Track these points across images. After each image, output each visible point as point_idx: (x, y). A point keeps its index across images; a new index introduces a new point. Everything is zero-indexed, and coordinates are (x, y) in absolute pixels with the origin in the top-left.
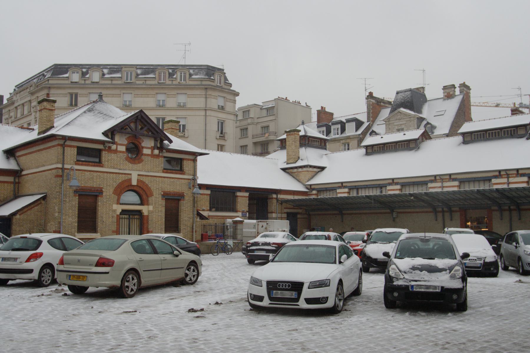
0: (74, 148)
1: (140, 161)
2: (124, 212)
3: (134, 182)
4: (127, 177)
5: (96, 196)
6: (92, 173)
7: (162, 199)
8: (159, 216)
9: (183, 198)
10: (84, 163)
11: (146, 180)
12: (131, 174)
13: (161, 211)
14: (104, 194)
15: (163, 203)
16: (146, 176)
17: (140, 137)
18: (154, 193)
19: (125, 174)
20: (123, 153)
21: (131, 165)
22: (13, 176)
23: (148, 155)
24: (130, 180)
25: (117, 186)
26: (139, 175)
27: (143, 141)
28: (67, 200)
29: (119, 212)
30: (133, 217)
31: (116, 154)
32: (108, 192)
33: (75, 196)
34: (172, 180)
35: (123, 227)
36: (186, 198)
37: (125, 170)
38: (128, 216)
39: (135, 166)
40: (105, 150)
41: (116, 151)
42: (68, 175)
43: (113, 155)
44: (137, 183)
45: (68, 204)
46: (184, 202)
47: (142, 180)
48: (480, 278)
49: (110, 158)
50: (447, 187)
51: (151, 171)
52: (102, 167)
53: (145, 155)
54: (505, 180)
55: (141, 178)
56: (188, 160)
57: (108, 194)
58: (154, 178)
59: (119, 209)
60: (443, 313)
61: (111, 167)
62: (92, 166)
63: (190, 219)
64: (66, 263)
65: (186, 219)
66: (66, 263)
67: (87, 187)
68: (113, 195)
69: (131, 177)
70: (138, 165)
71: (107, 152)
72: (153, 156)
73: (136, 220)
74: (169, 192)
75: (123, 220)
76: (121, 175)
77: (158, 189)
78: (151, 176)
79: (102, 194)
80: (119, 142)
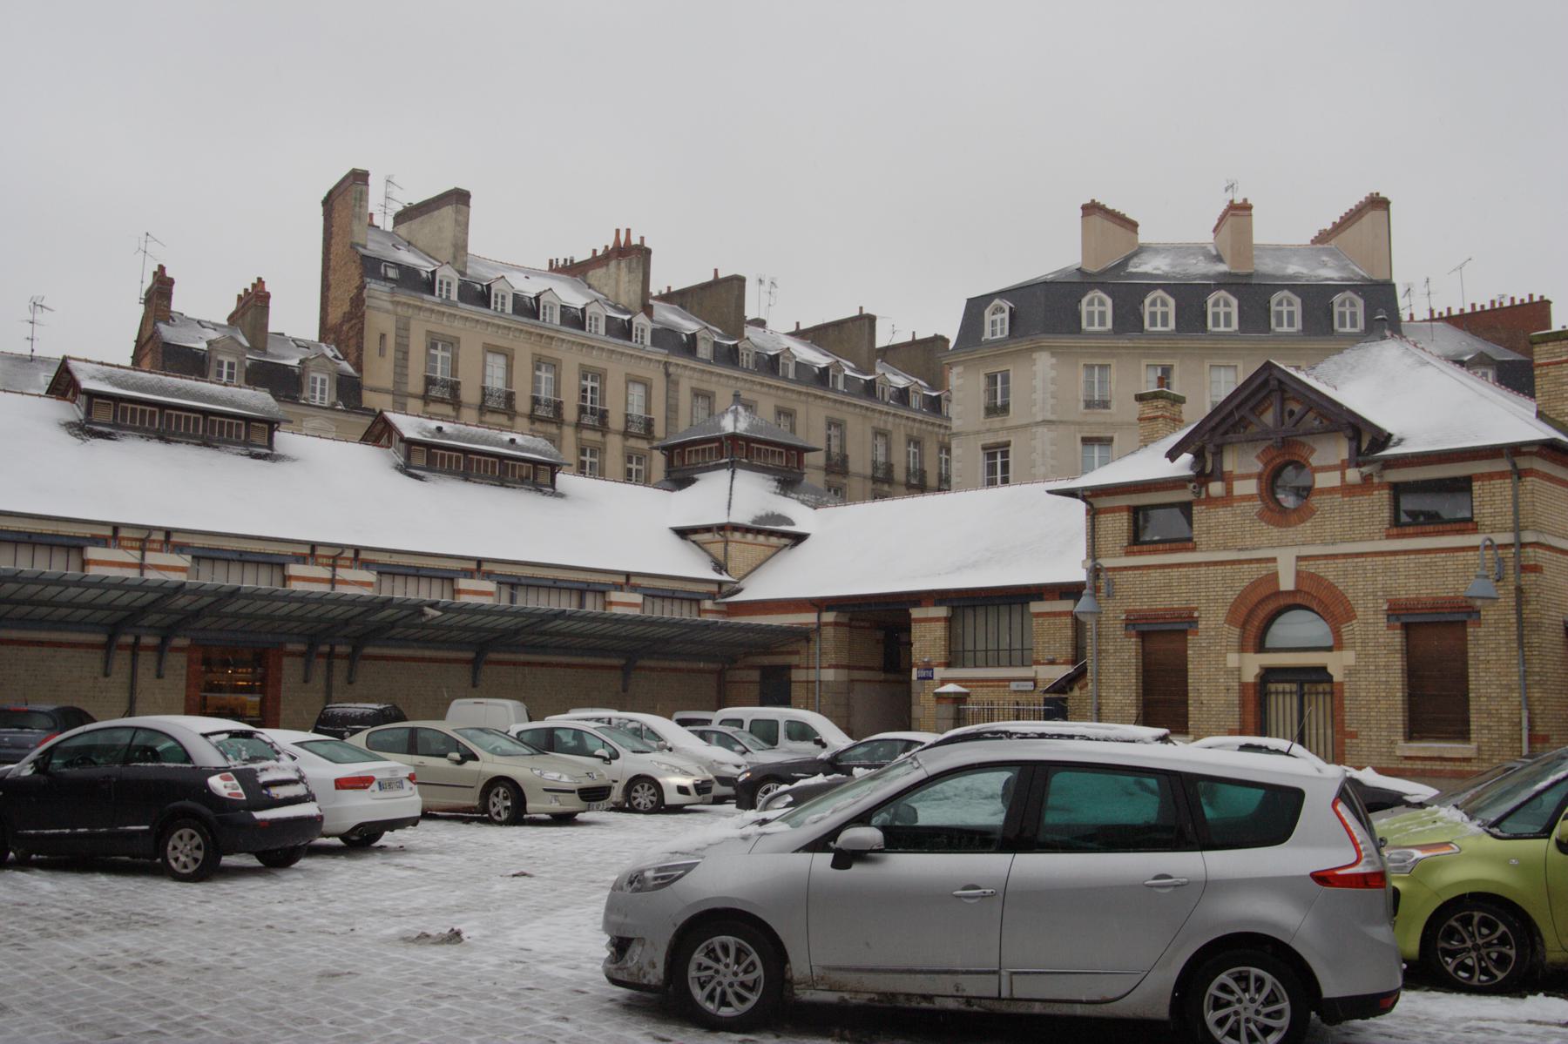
0: (1382, 492)
1: (1302, 514)
2: (1269, 674)
3: (1287, 583)
4: (1263, 570)
5: (1185, 632)
6: (1388, 558)
7: (1389, 627)
8: (1378, 683)
9: (1474, 616)
10: (1161, 547)
11: (1328, 571)
12: (1274, 560)
13: (1387, 667)
14: (1202, 625)
15: (1396, 638)
16: (1326, 557)
17: (1302, 439)
18: (1360, 611)
19: (1259, 561)
20: (1249, 500)
21: (1275, 532)
22: (814, 611)
23: (1332, 490)
24: (1274, 577)
25: (1236, 599)
26: (1299, 558)
27: (1313, 451)
28: (1111, 648)
29: (1250, 675)
30: (1313, 690)
31: (1229, 509)
32: (1214, 622)
33: (1127, 636)
34: (1427, 558)
35: (1281, 723)
36: (1489, 615)
37: (1258, 548)
38: (1294, 687)
39: (1290, 533)
40: (1199, 502)
41: (1228, 499)
42: (1111, 583)
43: (1221, 511)
44: (1297, 583)
45: (1111, 660)
46: (1481, 631)
47: (1313, 571)
48: (1493, 998)
49: (1213, 522)
50: (345, 582)
51: (1343, 541)
52: (1194, 549)
53: (1323, 491)
54: (132, 556)
55: (1310, 567)
56: (1491, 476)
57: (1212, 624)
58: (1356, 560)
59: (1252, 665)
60: (654, 1017)
61: (1218, 548)
62: (1165, 551)
63: (1511, 690)
64: (573, 792)
65: (1493, 691)
66: (573, 792)
67: (1156, 610)
68: (1226, 626)
69: (1297, 565)
70: (1300, 527)
71: (1204, 507)
72: (1347, 490)
73: (1288, 697)
74: (1417, 599)
75: (1314, 697)
76: (1246, 566)
77: (1374, 594)
78: (1346, 556)
79: (1197, 628)
80: (1237, 472)
